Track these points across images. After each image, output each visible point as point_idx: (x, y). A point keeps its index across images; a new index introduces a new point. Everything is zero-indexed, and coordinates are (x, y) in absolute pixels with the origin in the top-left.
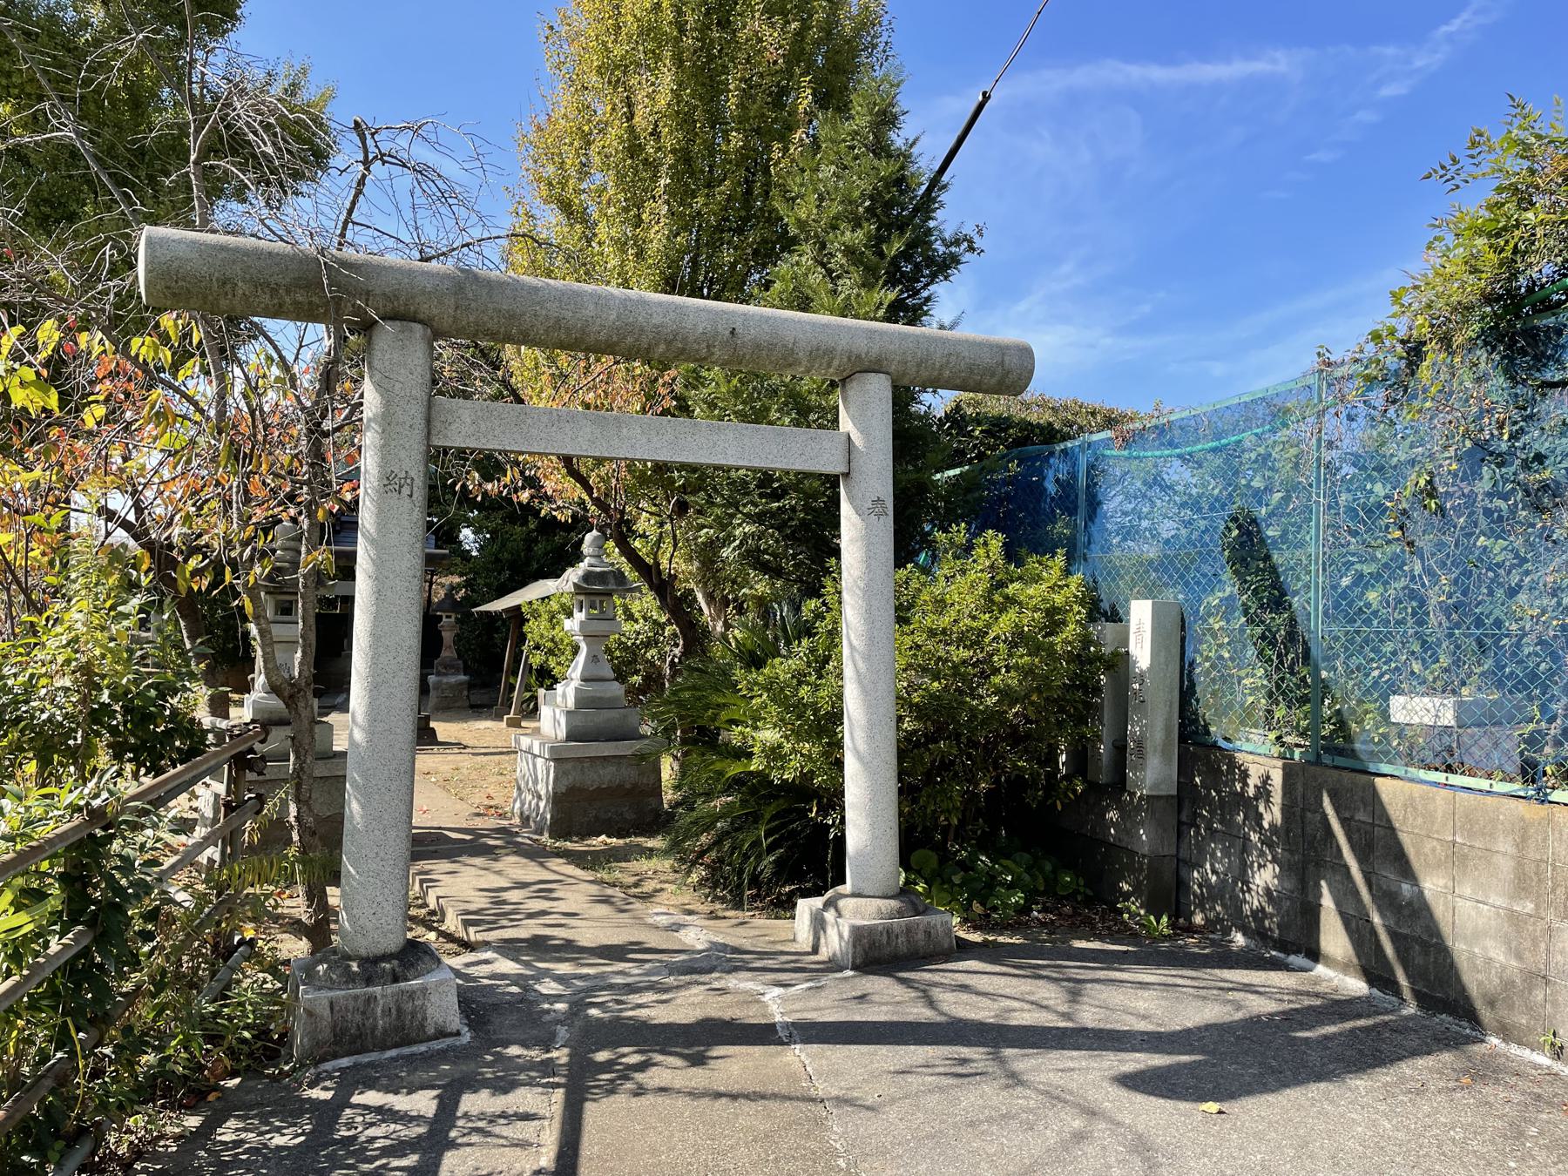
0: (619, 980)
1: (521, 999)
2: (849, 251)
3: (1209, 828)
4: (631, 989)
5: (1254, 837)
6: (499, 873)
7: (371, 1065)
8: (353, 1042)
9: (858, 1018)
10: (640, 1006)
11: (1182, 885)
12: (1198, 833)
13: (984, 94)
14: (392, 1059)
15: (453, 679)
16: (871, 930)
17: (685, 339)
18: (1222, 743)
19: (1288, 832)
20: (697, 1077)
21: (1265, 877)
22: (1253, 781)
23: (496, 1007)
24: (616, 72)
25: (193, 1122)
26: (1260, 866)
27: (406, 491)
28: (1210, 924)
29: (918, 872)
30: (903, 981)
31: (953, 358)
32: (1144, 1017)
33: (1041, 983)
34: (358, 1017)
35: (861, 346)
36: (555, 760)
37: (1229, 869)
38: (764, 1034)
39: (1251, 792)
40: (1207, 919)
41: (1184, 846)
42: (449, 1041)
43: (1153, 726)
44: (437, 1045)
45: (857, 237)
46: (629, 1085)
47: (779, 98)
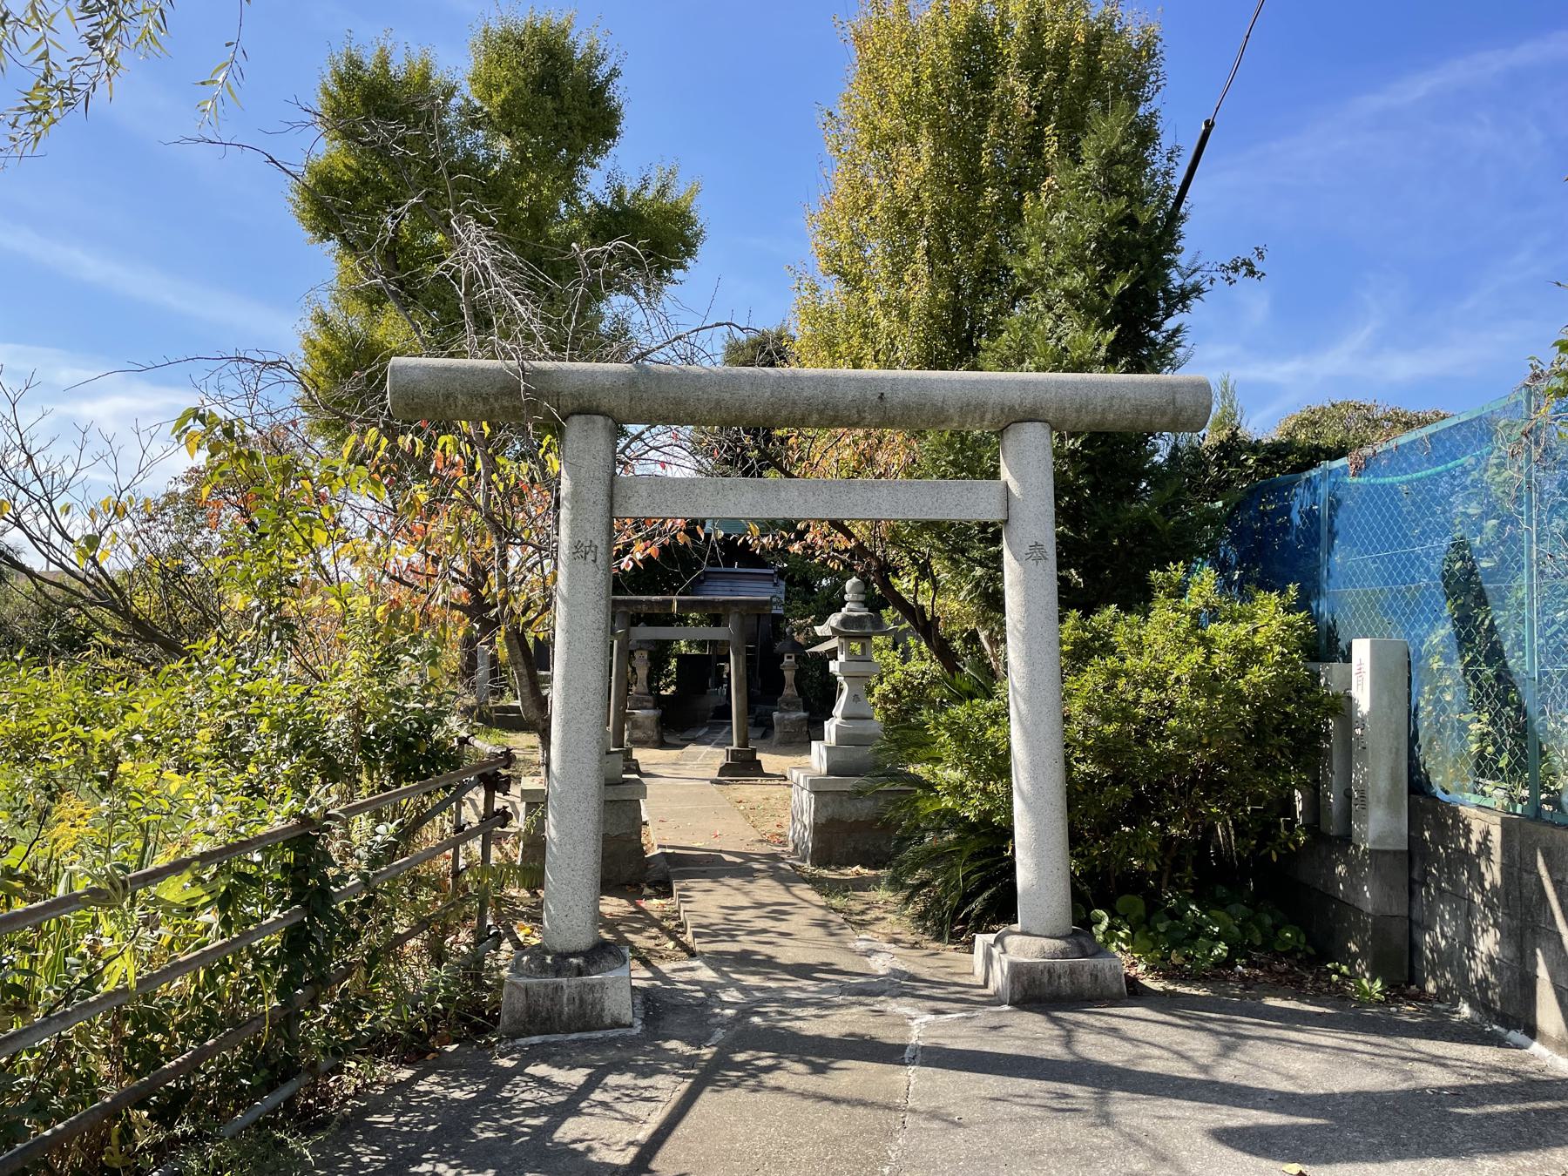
0: (794, 995)
1: (703, 1004)
2: (1070, 295)
3: (1438, 888)
4: (799, 1003)
5: (1477, 898)
6: (747, 894)
7: (554, 1044)
8: (543, 1023)
9: (987, 1049)
10: (798, 1018)
11: (1414, 948)
12: (1428, 893)
13: (1207, 123)
14: (574, 1041)
15: (794, 716)
16: (1030, 968)
17: (835, 408)
18: (1441, 795)
19: (1507, 894)
20: (813, 1083)
21: (1488, 943)
22: (1475, 837)
23: (676, 1008)
24: (883, 142)
25: (406, 1074)
26: (1484, 931)
27: (590, 557)
28: (1440, 996)
29: (1124, 918)
30: (1055, 1021)
31: (1116, 402)
32: (1290, 1078)
33: (1201, 1034)
34: (548, 1003)
35: (1014, 397)
36: (815, 792)
37: (1456, 933)
38: (891, 1054)
39: (1474, 848)
40: (1438, 987)
41: (1416, 907)
42: (622, 1031)
43: (1376, 775)
44: (611, 1033)
45: (1076, 280)
46: (752, 1082)
47: (1035, 146)
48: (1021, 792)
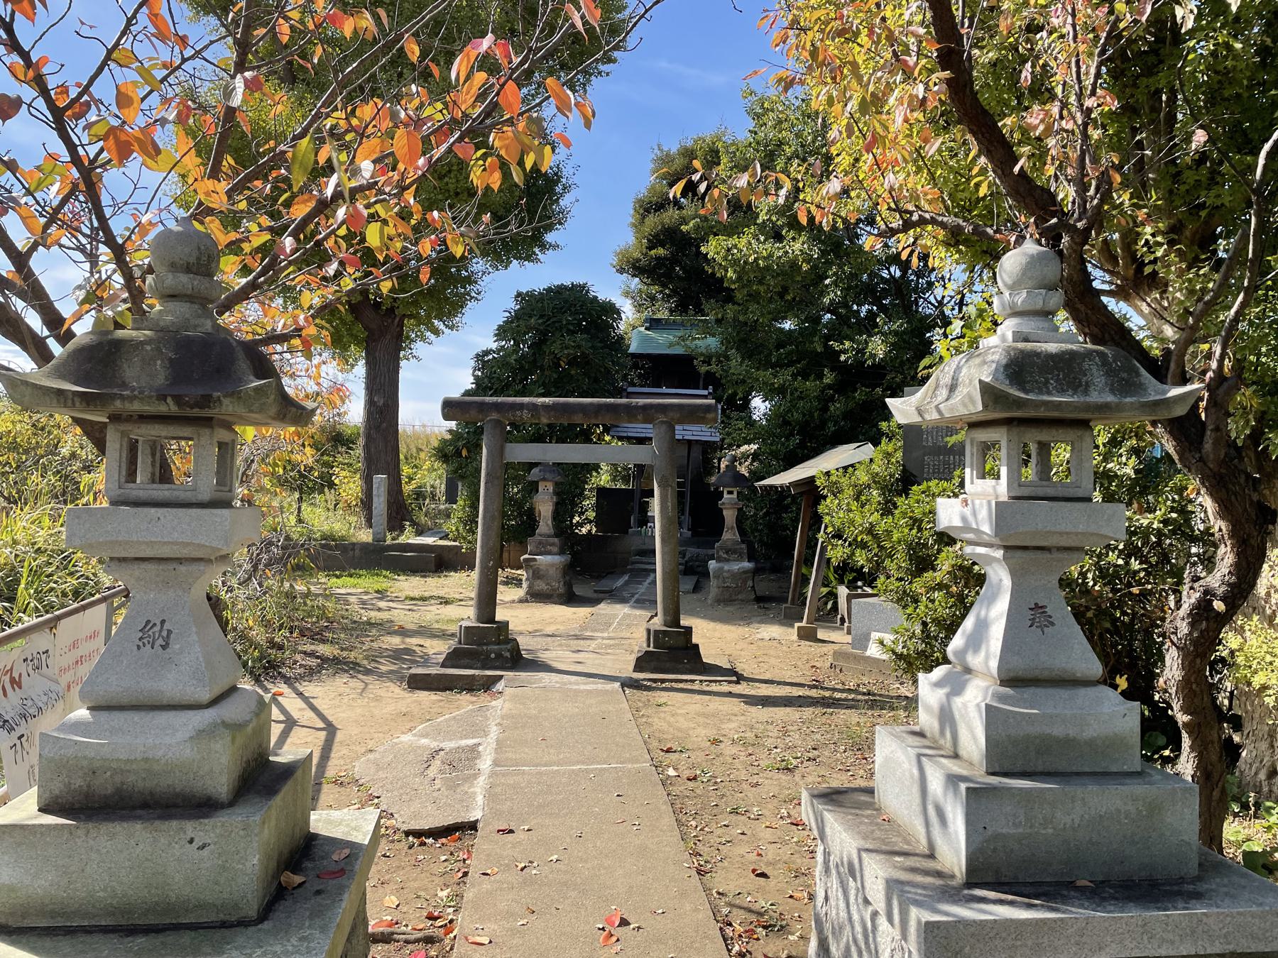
48: (964, 632)
